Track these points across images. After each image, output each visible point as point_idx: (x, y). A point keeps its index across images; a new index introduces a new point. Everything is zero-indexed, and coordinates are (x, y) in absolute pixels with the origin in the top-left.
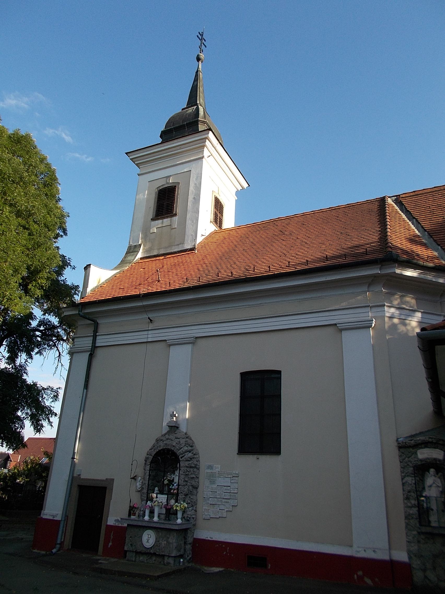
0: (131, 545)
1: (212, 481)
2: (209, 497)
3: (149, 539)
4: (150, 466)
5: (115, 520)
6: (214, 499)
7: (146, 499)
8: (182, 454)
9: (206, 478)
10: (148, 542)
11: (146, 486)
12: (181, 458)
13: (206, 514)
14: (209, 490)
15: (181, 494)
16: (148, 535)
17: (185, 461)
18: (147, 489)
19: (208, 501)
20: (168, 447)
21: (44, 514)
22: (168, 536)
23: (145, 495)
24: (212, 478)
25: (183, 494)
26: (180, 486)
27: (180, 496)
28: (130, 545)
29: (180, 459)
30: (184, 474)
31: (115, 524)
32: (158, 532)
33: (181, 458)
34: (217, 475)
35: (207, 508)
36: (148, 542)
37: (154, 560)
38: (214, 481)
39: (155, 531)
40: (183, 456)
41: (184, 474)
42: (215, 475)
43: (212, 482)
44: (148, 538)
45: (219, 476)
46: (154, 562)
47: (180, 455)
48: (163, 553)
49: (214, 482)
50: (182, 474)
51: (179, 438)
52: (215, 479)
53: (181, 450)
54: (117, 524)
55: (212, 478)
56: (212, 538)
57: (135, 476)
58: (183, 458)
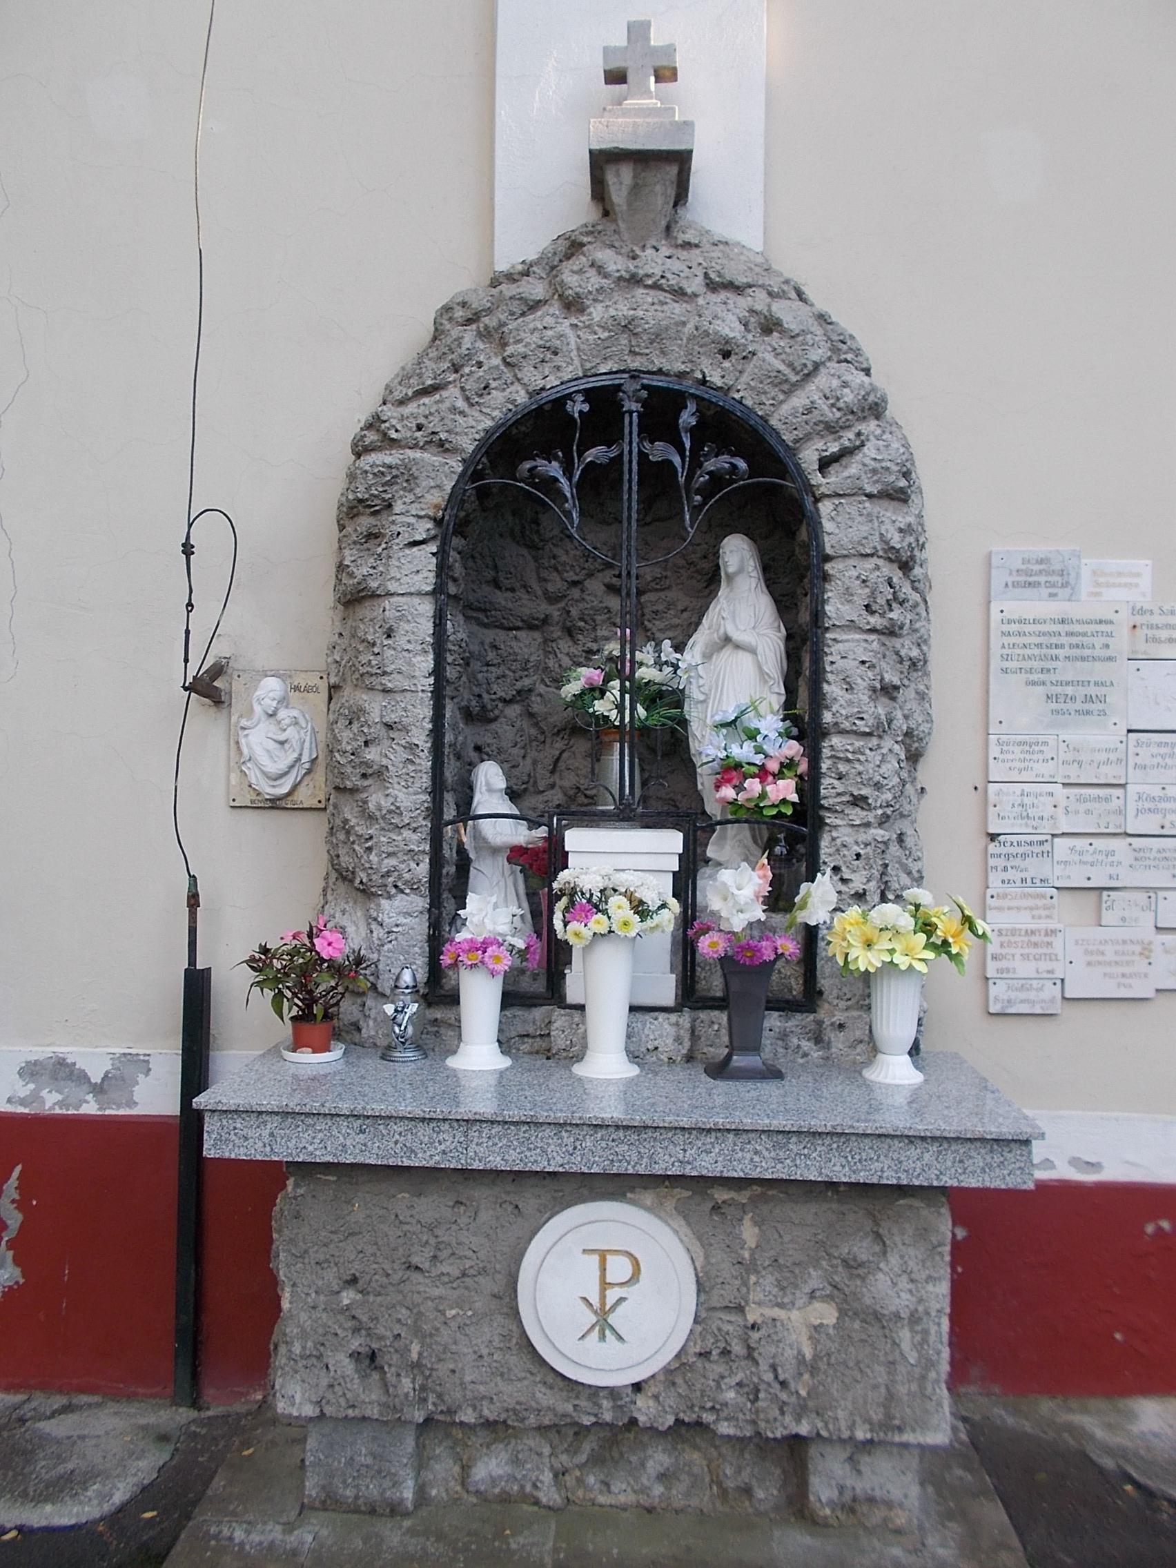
0: (370, 1360)
1: (1069, 690)
2: (1047, 828)
3: (612, 1295)
4: (441, 555)
5: (31, 1071)
6: (1099, 843)
7: (422, 870)
8: (831, 429)
9: (1005, 671)
10: (603, 1323)
11: (412, 747)
12: (825, 464)
13: (1025, 969)
14: (1045, 770)
15: (857, 815)
16: (603, 1255)
17: (870, 496)
18: (425, 781)
19: (1036, 868)
20: (659, 362)
21: (618, 175)
22: (862, 1249)
23: (418, 841)
24: (1068, 672)
25: (870, 817)
26: (836, 740)
27: (844, 834)
28: (348, 1367)
29: (816, 479)
30: (875, 621)
31: (35, 1097)
32: (716, 1208)
33: (825, 464)
34: (1122, 642)
35: (1024, 921)
36: (603, 1323)
37: (663, 1477)
38: (1092, 691)
39: (670, 1205)
40: (845, 453)
41: (875, 621)
42: (1099, 641)
43: (1074, 699)
44: (604, 1285)
45: (1143, 648)
46: (658, 1490)
47: (808, 437)
48: (798, 1419)
49: (1089, 699)
50: (852, 626)
51: (741, 280)
52: (1099, 671)
53: (811, 387)
54: (51, 1102)
55: (1068, 672)
56: (1094, 1166)
57: (218, 670)
58: (853, 468)
